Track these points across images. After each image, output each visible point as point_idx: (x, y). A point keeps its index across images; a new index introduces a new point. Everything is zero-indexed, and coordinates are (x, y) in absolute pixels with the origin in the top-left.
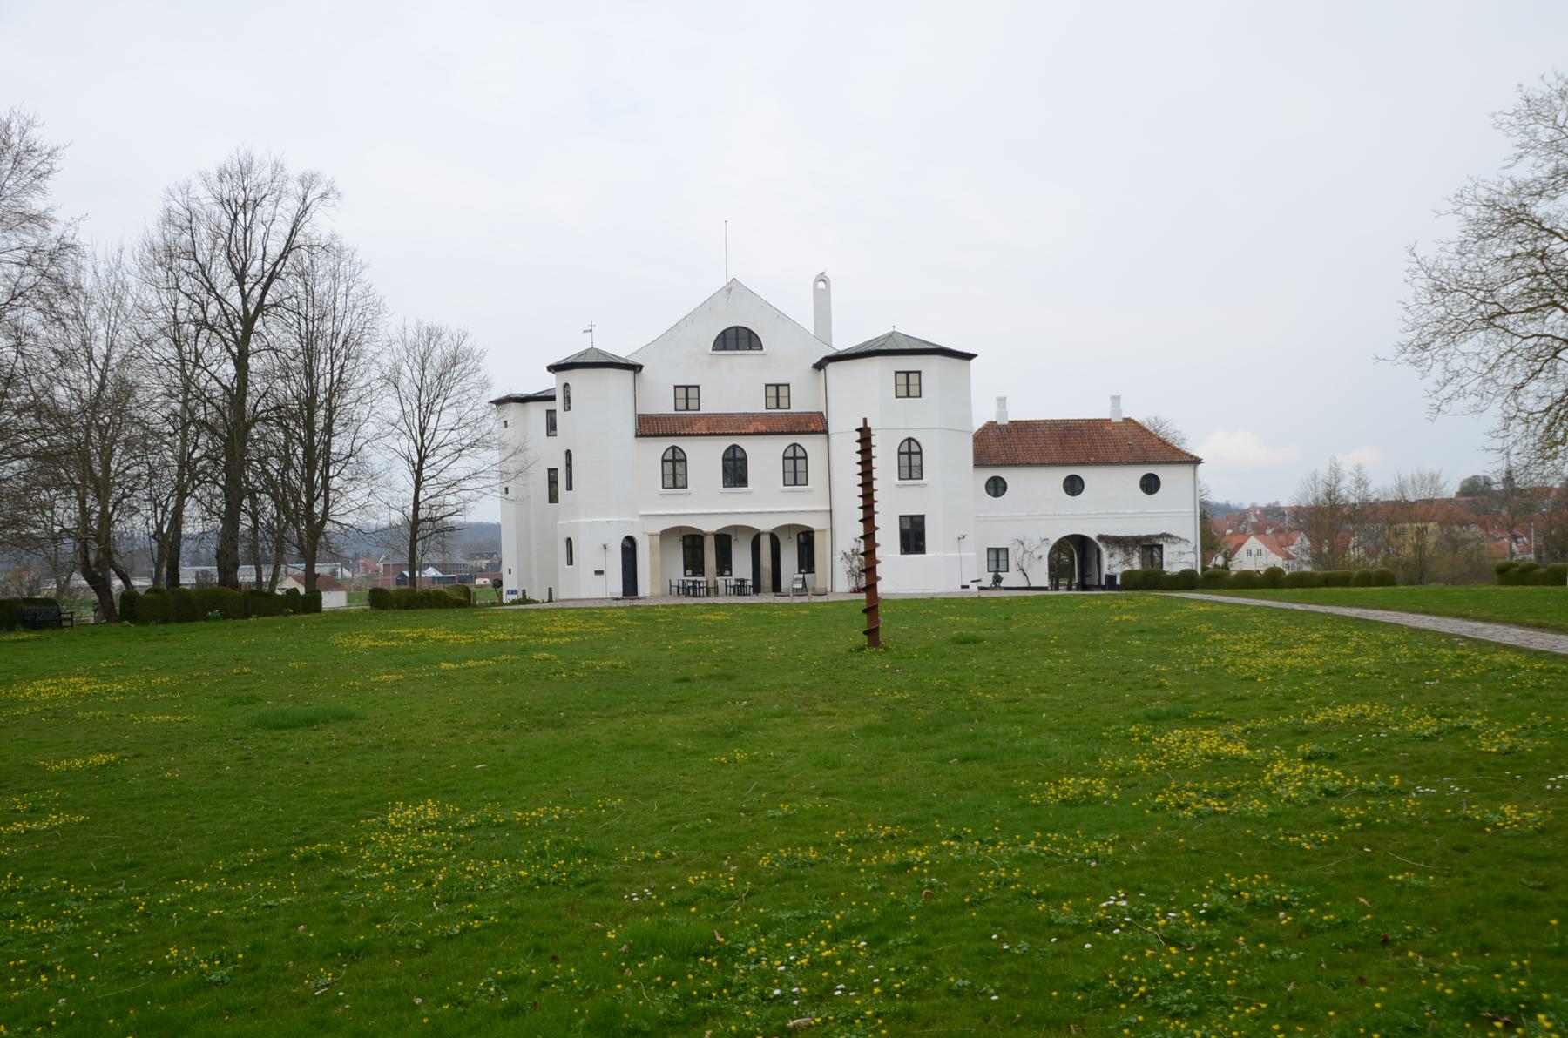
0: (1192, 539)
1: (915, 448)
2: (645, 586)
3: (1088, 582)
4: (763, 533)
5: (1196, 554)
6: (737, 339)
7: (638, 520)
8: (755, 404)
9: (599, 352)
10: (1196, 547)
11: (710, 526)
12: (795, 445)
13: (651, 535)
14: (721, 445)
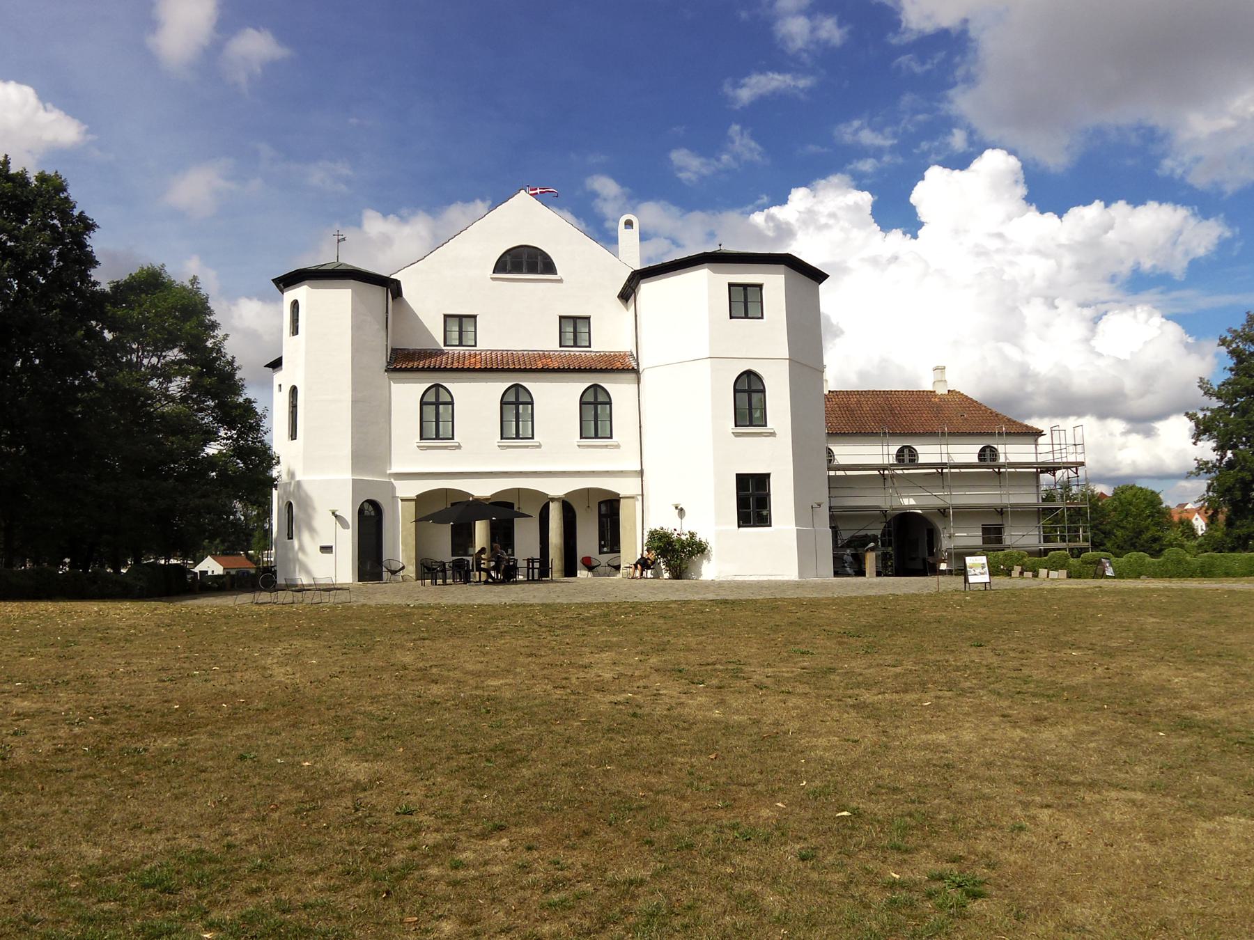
4: (553, 499)
8: (546, 340)
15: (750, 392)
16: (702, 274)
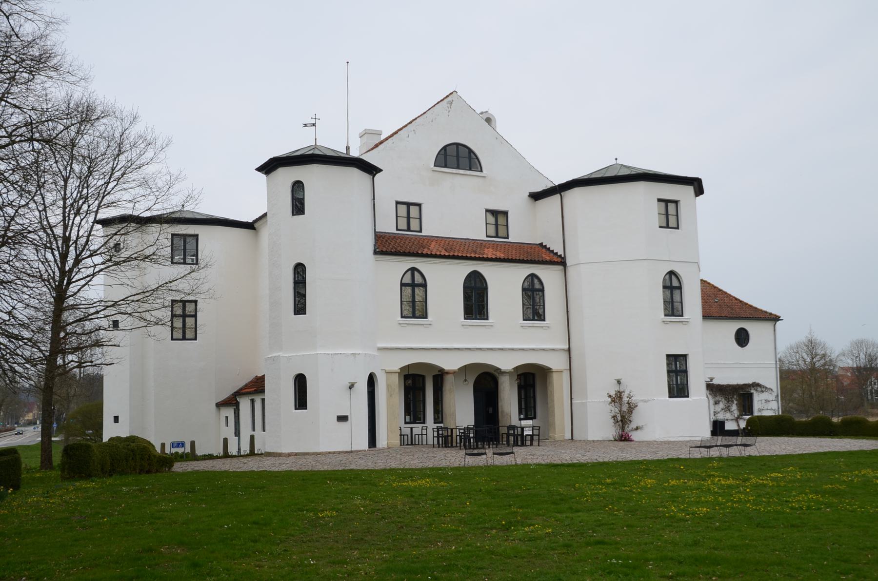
0: (775, 389)
2: (382, 441)
5: (778, 402)
6: (458, 157)
7: (376, 353)
10: (777, 396)
11: (507, 363)
12: (413, 270)
13: (388, 373)
14: (464, 269)
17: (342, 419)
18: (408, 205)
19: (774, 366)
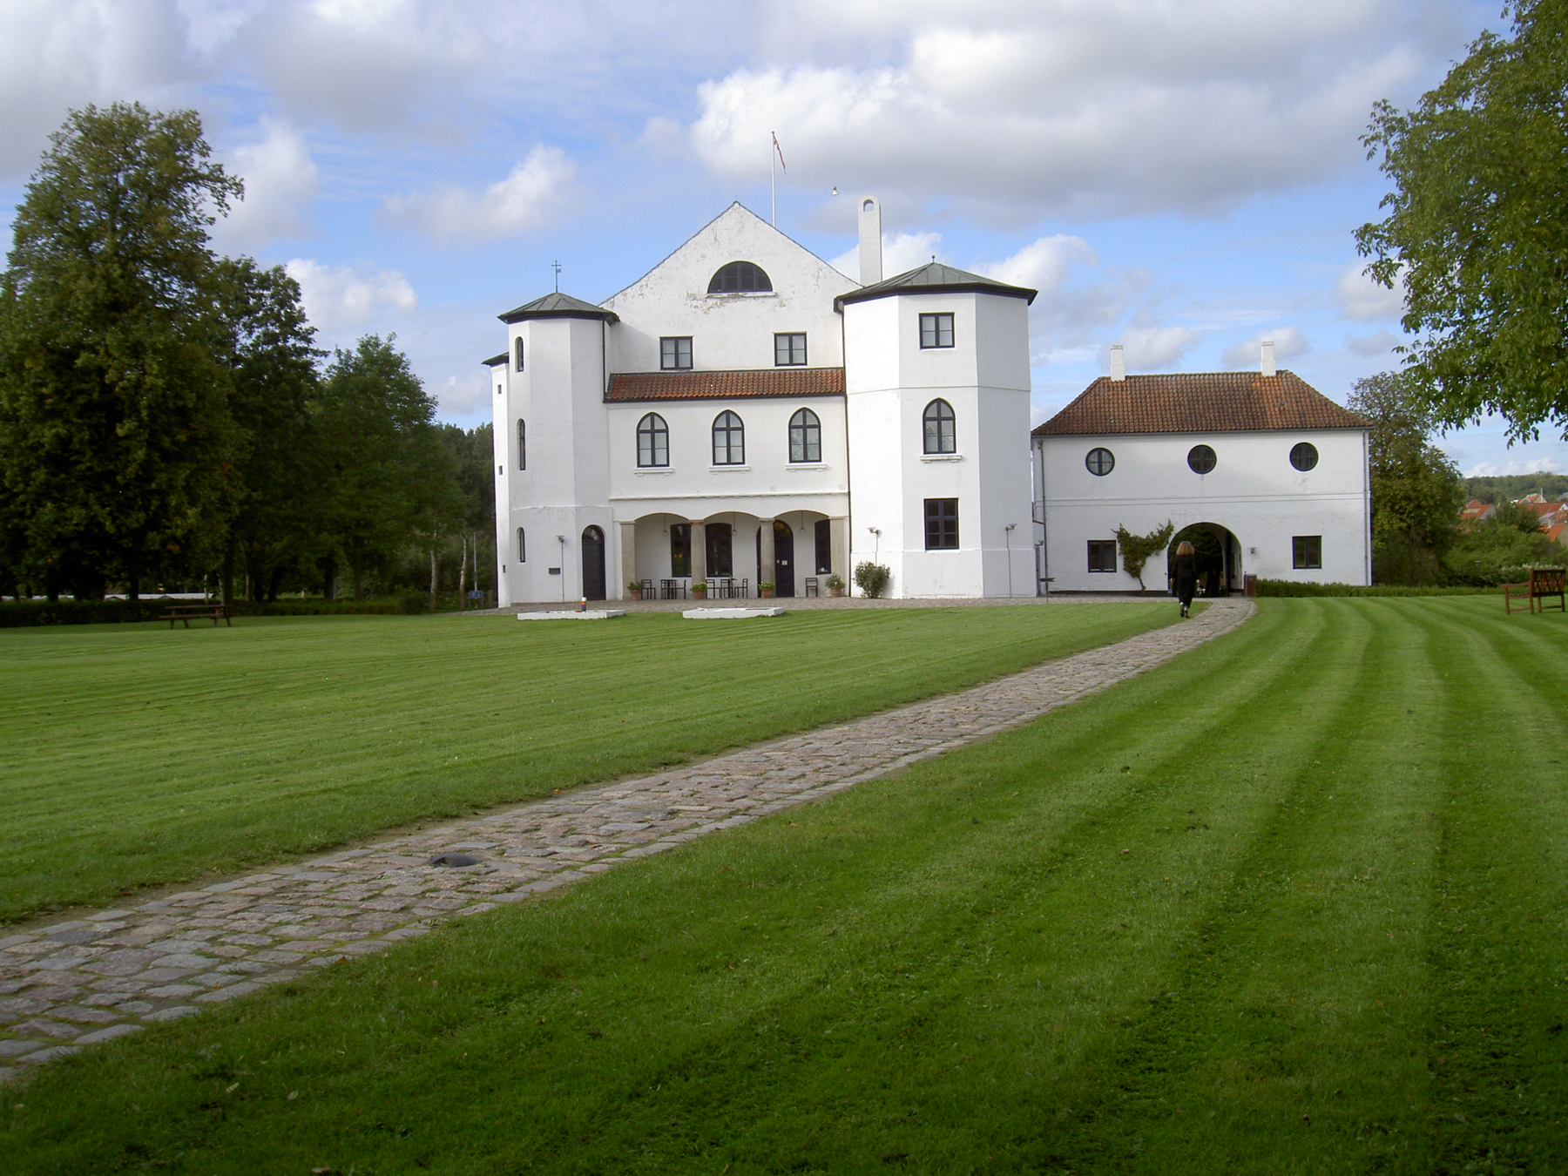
1: (945, 413)
3: (1234, 587)
4: (763, 521)
8: (762, 359)
9: (563, 298)
11: (696, 513)
15: (939, 419)
16: (894, 301)
17: (555, 571)
18: (790, 336)
19: (1362, 496)
